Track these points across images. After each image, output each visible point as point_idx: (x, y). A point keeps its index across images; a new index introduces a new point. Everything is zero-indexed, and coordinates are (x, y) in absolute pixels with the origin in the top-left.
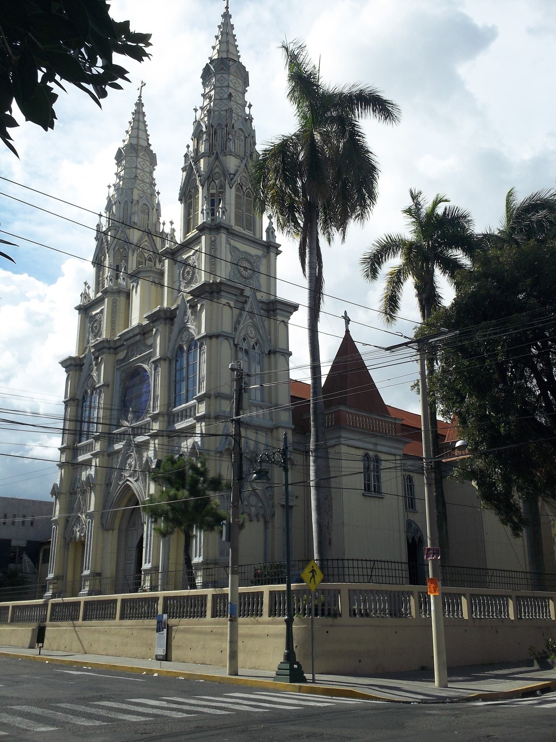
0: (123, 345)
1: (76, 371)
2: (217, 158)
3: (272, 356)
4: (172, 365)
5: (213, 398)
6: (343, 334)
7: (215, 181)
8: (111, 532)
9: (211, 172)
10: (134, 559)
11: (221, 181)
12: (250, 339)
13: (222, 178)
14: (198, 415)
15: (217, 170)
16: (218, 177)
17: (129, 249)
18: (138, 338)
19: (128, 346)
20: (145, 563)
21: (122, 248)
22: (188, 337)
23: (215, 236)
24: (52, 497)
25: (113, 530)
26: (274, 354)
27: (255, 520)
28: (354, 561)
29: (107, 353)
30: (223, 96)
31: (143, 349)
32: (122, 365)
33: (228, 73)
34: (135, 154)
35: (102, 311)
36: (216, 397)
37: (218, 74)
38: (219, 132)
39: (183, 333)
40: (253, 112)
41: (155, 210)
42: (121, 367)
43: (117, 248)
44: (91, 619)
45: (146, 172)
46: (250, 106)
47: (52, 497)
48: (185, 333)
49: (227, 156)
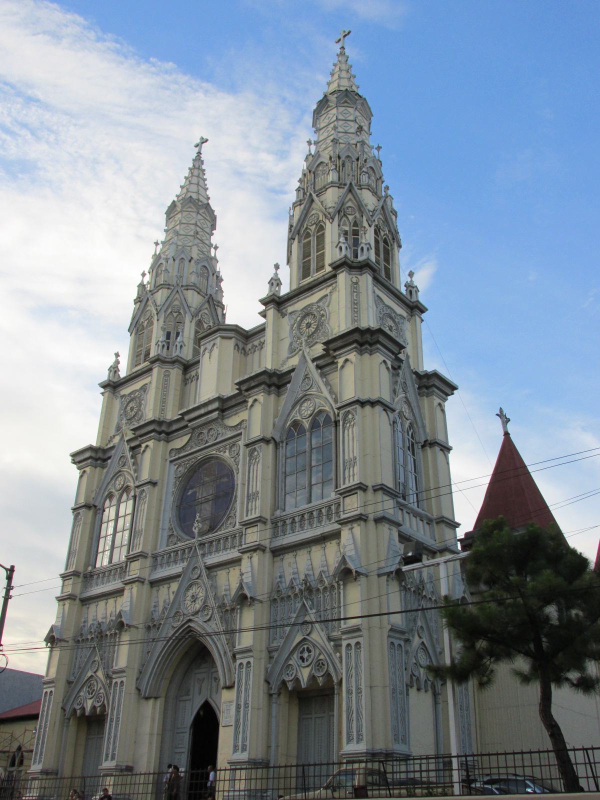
0: (186, 426)
1: (96, 467)
2: (350, 190)
3: (428, 448)
5: (370, 491)
7: (348, 216)
8: (151, 701)
9: (343, 204)
10: (187, 746)
11: (355, 217)
13: (357, 215)
14: (343, 516)
15: (350, 204)
17: (185, 313)
18: (215, 415)
19: (193, 429)
20: (106, 760)
22: (311, 409)
25: (156, 698)
26: (430, 447)
28: (491, 757)
34: (195, 210)
35: (144, 389)
36: (375, 491)
38: (348, 164)
39: (302, 404)
40: (219, 254)
43: (170, 311)
46: (216, 248)
48: (305, 404)
49: (363, 190)
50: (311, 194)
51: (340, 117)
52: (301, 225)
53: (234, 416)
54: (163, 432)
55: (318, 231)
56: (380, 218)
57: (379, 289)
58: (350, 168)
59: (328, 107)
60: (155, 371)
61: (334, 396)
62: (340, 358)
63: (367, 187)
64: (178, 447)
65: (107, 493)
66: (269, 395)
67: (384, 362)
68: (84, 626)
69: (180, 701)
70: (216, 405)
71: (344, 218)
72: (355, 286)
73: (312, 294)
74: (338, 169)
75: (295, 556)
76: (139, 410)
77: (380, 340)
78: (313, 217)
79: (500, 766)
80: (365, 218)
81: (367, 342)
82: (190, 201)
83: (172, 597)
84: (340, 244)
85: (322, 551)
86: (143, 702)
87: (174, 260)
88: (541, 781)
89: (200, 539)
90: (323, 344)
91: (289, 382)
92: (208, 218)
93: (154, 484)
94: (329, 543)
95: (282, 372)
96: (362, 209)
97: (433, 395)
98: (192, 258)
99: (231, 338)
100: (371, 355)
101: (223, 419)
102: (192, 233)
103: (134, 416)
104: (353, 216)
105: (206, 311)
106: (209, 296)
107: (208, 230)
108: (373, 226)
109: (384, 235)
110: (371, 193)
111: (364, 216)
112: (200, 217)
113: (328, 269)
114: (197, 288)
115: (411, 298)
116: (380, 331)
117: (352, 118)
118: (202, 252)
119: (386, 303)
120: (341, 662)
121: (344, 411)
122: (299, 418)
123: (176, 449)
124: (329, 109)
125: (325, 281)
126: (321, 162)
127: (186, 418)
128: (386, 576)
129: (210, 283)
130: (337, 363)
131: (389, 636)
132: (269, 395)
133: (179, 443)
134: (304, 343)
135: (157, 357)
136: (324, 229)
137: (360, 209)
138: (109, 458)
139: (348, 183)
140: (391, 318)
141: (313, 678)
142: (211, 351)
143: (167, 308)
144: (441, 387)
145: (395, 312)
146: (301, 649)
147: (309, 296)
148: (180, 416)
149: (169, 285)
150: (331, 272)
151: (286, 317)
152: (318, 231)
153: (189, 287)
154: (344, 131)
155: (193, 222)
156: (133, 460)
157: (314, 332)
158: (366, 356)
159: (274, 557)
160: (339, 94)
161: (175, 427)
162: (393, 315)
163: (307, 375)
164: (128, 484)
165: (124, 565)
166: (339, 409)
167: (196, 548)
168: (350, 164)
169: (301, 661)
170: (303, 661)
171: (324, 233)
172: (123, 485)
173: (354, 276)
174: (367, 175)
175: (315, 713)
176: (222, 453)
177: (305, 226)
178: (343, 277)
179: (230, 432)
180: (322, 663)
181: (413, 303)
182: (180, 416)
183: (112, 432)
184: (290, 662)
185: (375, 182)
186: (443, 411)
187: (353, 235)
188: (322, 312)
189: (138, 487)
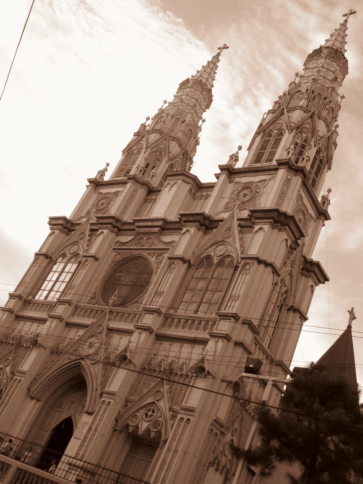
0: (134, 230)
1: (62, 233)
2: (311, 117)
6: (345, 328)
7: (303, 133)
8: (34, 402)
9: (302, 125)
11: (307, 136)
12: (284, 285)
13: (309, 135)
14: (214, 331)
15: (307, 126)
16: (306, 132)
17: (165, 155)
18: (157, 230)
19: (138, 233)
23: (292, 175)
25: (38, 400)
26: (293, 312)
27: (219, 472)
29: (110, 231)
30: (327, 76)
34: (200, 90)
35: (116, 194)
37: (329, 59)
38: (317, 99)
41: (195, 139)
43: (155, 149)
45: (201, 107)
46: (204, 121)
48: (221, 247)
50: (283, 109)
51: (325, 66)
53: (168, 236)
55: (278, 136)
60: (129, 185)
61: (242, 249)
62: (257, 225)
63: (324, 119)
65: (62, 253)
66: (199, 231)
67: (287, 240)
68: (11, 333)
69: (53, 410)
70: (160, 223)
71: (299, 134)
72: (288, 181)
74: (309, 100)
75: (171, 345)
76: (107, 207)
78: (279, 124)
80: (313, 139)
81: (280, 222)
83: (77, 338)
84: (289, 150)
86: (29, 399)
87: (172, 117)
89: (112, 308)
91: (216, 228)
92: (207, 100)
93: (96, 259)
94: (197, 346)
95: (214, 219)
96: (314, 133)
97: (310, 277)
98: (185, 121)
99: (188, 183)
100: (279, 231)
101: (160, 235)
103: (102, 209)
104: (306, 135)
105: (179, 160)
106: (185, 150)
107: (203, 107)
109: (322, 156)
111: (313, 138)
112: (201, 96)
113: (274, 163)
114: (180, 142)
116: (292, 218)
119: (304, 202)
120: (172, 427)
121: (245, 261)
122: (212, 254)
123: (121, 242)
124: (320, 57)
128: (226, 384)
129: (190, 142)
130: (254, 228)
131: (212, 424)
134: (237, 206)
135: (133, 176)
137: (313, 133)
138: (74, 230)
139: (312, 111)
140: (304, 214)
141: (148, 430)
142: (172, 186)
144: (318, 275)
145: (307, 211)
146: (149, 408)
148: (133, 221)
149: (162, 132)
150: (275, 165)
151: (232, 184)
152: (278, 136)
156: (89, 238)
158: (276, 231)
159: (156, 340)
160: (331, 50)
161: (126, 227)
162: (306, 212)
163: (230, 228)
164: (79, 252)
166: (242, 258)
168: (318, 100)
169: (145, 416)
170: (146, 417)
172: (76, 252)
173: (290, 175)
174: (327, 111)
176: (150, 257)
177: (271, 129)
178: (282, 172)
181: (322, 210)
182: (133, 221)
183: (83, 214)
184: (138, 414)
185: (331, 118)
186: (312, 291)
187: (301, 148)
189: (85, 256)
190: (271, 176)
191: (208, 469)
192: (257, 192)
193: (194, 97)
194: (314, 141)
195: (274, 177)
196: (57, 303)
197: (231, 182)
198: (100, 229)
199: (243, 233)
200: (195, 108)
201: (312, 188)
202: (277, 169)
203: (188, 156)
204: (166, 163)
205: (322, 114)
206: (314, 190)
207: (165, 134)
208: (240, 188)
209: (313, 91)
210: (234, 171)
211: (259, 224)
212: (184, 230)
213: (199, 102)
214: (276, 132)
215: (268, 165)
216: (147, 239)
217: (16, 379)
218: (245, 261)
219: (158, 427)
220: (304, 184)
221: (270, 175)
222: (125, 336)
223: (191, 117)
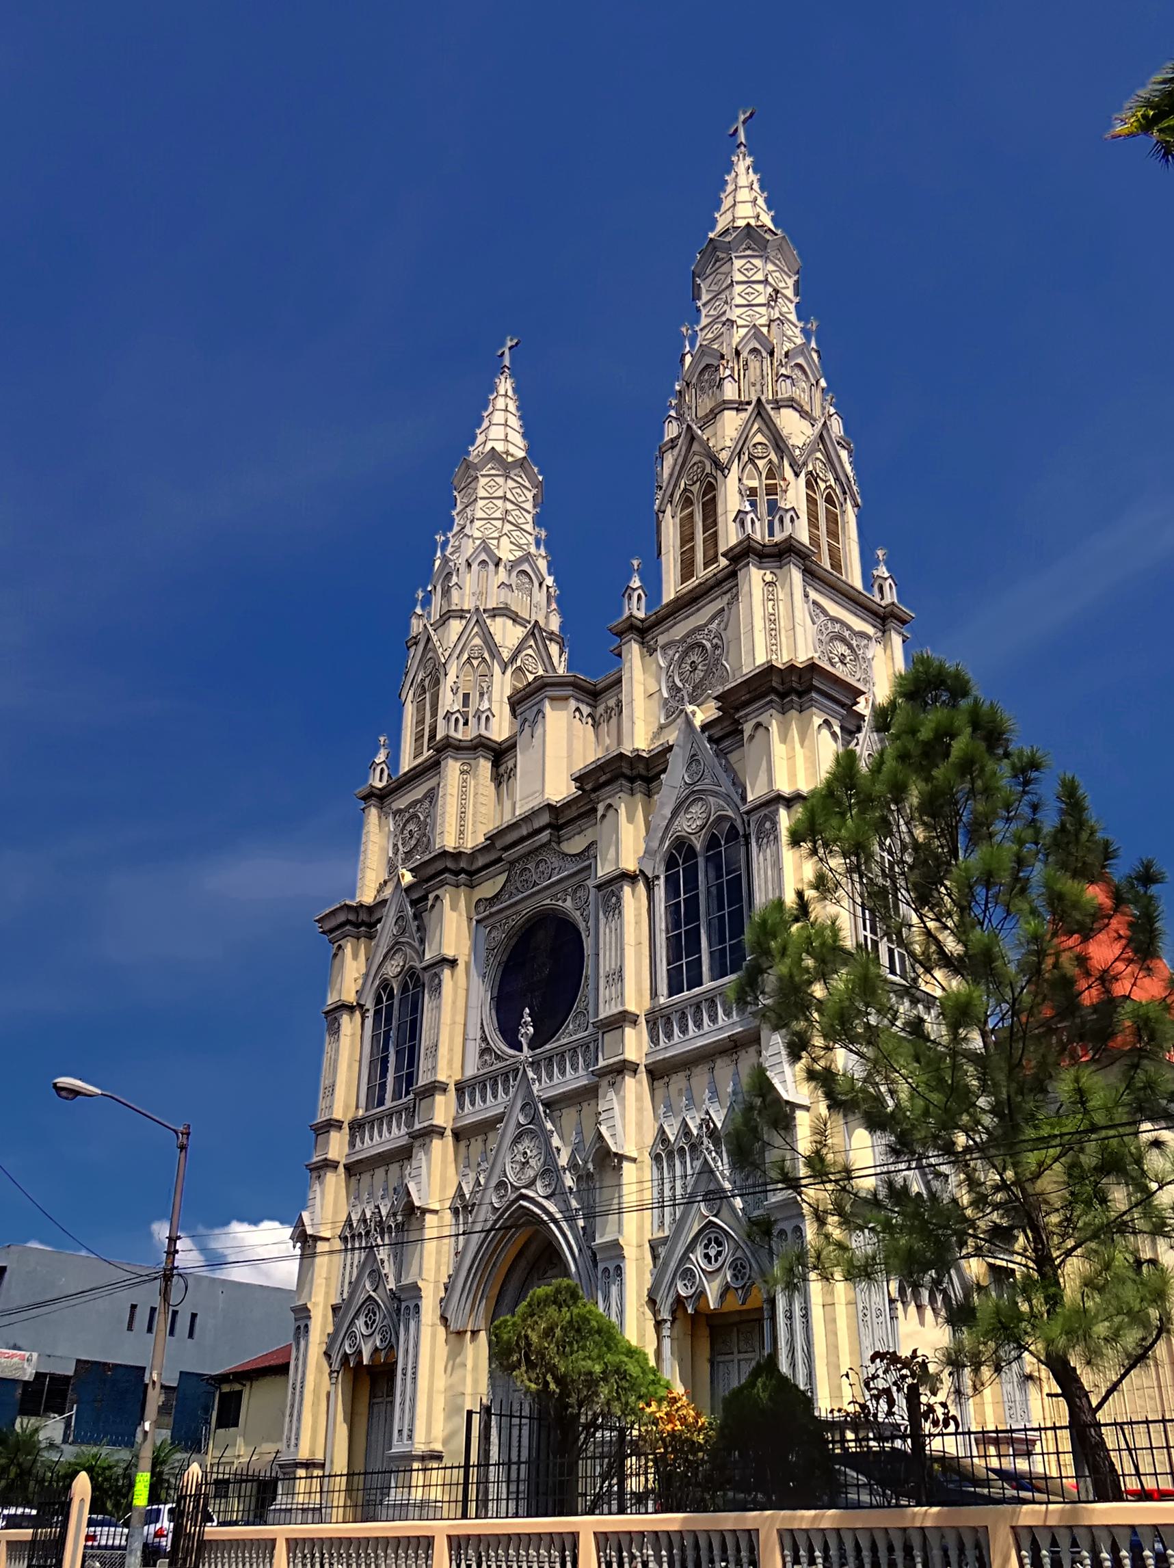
0: (500, 860)
1: (358, 939)
4: (656, 889)
7: (756, 461)
13: (773, 456)
18: (545, 836)
19: (512, 863)
21: (477, 658)
24: (294, 1247)
31: (556, 865)
32: (494, 909)
33: (761, 256)
42: (491, 915)
43: (466, 656)
44: (8, 1549)
47: (294, 1247)
52: (675, 486)
54: (463, 871)
56: (817, 459)
57: (816, 589)
58: (758, 371)
59: (716, 261)
61: (740, 791)
62: (747, 721)
63: (790, 403)
64: (489, 896)
66: (632, 795)
70: (545, 819)
73: (699, 610)
74: (736, 377)
75: (689, 1078)
77: (815, 683)
78: (695, 468)
79: (1060, 1450)
82: (493, 455)
85: (732, 1067)
88: (1044, 1482)
90: (715, 698)
91: (664, 771)
92: (527, 484)
94: (744, 1051)
98: (500, 559)
100: (801, 712)
101: (559, 843)
102: (498, 515)
105: (530, 651)
106: (533, 622)
108: (803, 475)
109: (827, 488)
110: (797, 415)
112: (511, 484)
115: (882, 599)
116: (812, 667)
117: (760, 277)
118: (519, 546)
119: (832, 613)
121: (758, 816)
123: (486, 900)
124: (718, 264)
125: (719, 583)
126: (707, 365)
127: (499, 844)
130: (742, 732)
132: (632, 795)
133: (488, 889)
134: (686, 698)
135: (444, 741)
136: (714, 489)
138: (379, 921)
140: (843, 640)
143: (461, 652)
145: (849, 628)
147: (692, 614)
148: (489, 842)
149: (462, 610)
150: (727, 567)
153: (496, 612)
154: (745, 302)
155: (500, 493)
156: (416, 923)
157: (702, 679)
159: (653, 1080)
161: (480, 862)
162: (847, 634)
163: (694, 755)
164: (411, 963)
165: (412, 1105)
167: (524, 1070)
168: (758, 364)
171: (714, 497)
172: (404, 966)
173: (768, 572)
174: (788, 381)
175: (739, 1352)
177: (682, 486)
179: (573, 865)
180: (741, 1264)
185: (807, 390)
187: (767, 495)
188: (715, 641)
190: (729, 595)
191: (893, 1318)
192: (716, 647)
193: (495, 495)
194: (791, 465)
195: (737, 595)
196: (415, 1099)
197: (651, 651)
198: (430, 892)
199: (726, 754)
200: (510, 518)
201: (839, 575)
202: (733, 575)
203: (545, 631)
204: (503, 673)
205: (779, 393)
206: (844, 578)
207: (469, 611)
208: (677, 655)
209: (736, 349)
210: (646, 624)
211: (749, 718)
212: (601, 808)
213: (512, 499)
214: (695, 488)
215: (710, 575)
216: (537, 867)
217: (407, 1308)
218: (758, 816)
219: (745, 1274)
220: (811, 574)
221: (725, 593)
222: (586, 1103)
223: (511, 542)
